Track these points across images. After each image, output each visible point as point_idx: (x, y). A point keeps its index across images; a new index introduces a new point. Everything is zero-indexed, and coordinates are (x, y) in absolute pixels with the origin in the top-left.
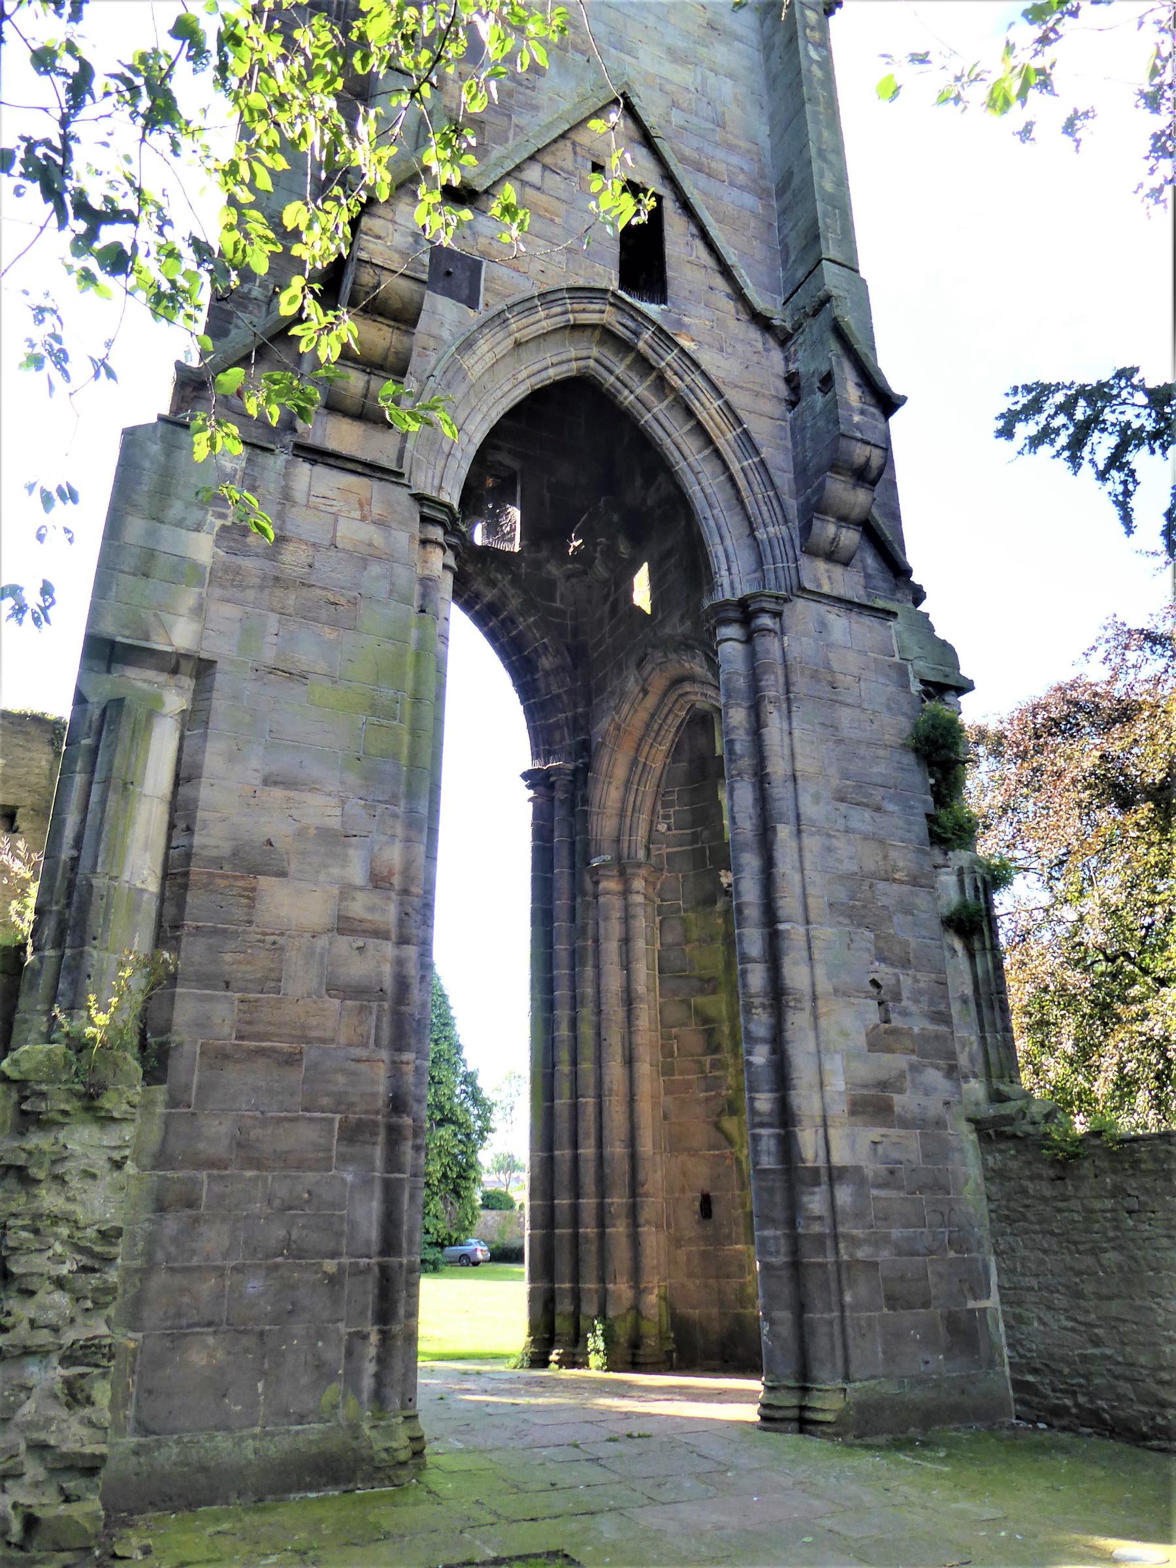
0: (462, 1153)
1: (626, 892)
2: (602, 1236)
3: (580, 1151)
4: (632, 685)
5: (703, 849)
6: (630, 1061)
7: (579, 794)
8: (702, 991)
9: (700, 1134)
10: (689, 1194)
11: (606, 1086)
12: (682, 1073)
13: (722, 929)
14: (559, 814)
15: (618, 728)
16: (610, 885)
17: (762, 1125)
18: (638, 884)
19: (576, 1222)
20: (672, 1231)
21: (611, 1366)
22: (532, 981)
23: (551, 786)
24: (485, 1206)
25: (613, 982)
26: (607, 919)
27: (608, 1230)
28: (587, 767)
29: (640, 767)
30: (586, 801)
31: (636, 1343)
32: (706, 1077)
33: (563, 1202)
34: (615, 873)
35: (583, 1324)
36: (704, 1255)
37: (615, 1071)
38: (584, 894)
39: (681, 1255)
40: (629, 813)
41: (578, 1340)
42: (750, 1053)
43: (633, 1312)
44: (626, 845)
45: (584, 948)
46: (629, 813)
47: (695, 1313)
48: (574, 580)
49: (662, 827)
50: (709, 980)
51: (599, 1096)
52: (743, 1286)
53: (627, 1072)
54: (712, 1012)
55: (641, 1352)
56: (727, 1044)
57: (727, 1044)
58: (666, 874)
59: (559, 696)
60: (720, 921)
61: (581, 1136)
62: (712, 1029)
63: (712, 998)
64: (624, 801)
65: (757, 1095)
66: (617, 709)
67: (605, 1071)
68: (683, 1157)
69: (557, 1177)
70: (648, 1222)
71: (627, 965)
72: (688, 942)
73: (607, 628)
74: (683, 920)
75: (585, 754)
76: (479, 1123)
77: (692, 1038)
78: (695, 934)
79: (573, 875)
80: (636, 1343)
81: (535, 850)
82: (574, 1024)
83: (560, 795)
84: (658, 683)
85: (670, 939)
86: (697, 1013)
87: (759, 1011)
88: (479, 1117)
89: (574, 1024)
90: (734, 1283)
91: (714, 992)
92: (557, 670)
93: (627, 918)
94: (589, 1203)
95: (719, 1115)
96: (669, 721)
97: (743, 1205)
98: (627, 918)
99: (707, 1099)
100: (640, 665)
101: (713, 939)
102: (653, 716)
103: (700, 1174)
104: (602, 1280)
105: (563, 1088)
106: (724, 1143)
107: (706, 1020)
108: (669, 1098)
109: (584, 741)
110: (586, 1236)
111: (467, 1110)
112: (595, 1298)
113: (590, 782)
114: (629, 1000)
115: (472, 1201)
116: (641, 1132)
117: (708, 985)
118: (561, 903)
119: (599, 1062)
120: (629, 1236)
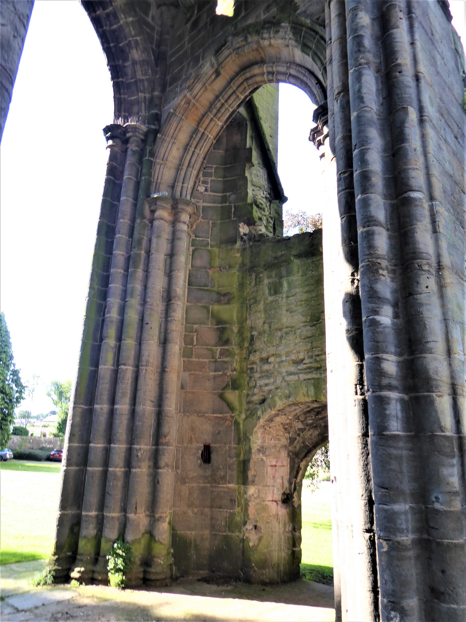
0: (6, 408)
1: (175, 222)
2: (128, 475)
3: (116, 406)
4: (207, 68)
5: (230, 207)
6: (164, 342)
7: (148, 148)
8: (219, 302)
9: (207, 401)
10: (195, 445)
11: (144, 359)
12: (198, 356)
13: (240, 260)
14: (130, 160)
15: (188, 102)
16: (163, 213)
17: (390, 387)
18: (185, 217)
19: (106, 463)
20: (179, 471)
21: (126, 585)
22: (92, 275)
23: (126, 141)
24: (14, 433)
25: (158, 283)
26: (158, 237)
27: (134, 470)
28: (156, 132)
29: (199, 135)
30: (152, 154)
31: (147, 562)
32: (216, 361)
33: (97, 445)
34: (169, 206)
35: (104, 546)
36: (203, 490)
37: (152, 349)
38: (143, 217)
39: (185, 489)
40: (185, 167)
41: (98, 558)
42: (376, 312)
43: (147, 536)
44: (179, 189)
45: (139, 255)
46: (185, 167)
47: (191, 534)
48: (164, 8)
49: (201, 189)
50: (225, 295)
51: (137, 366)
52: (232, 515)
53: (160, 350)
54: (225, 316)
55: (152, 570)
56: (235, 339)
57: (235, 339)
58: (200, 219)
59: (142, 81)
60: (238, 255)
61: (119, 394)
62: (224, 328)
63: (227, 307)
64: (182, 159)
65: (385, 356)
66: (190, 88)
67: (144, 347)
68: (194, 417)
69: (95, 425)
70: (167, 465)
71: (170, 274)
72: (211, 267)
73: (187, 39)
74: (210, 252)
75: (156, 126)
76: (18, 394)
77: (208, 333)
78: (217, 263)
79: (135, 205)
80: (147, 562)
81: (108, 182)
82: (122, 310)
83: (133, 147)
84: (230, 68)
85: (198, 263)
86: (213, 316)
87: (385, 273)
88: (17, 391)
89: (122, 310)
90: (225, 513)
91: (228, 302)
92: (143, 63)
93: (173, 240)
94: (119, 448)
95: (224, 389)
96: (230, 102)
97: (238, 455)
98: (173, 240)
99: (215, 377)
100: (218, 52)
101: (230, 267)
102: (217, 97)
103: (205, 431)
104: (124, 510)
105: (108, 358)
106: (226, 408)
107: (219, 322)
108: (187, 374)
109: (157, 114)
110: (115, 474)
111: (12, 388)
112: (117, 525)
113: (158, 141)
114: (168, 298)
115: (7, 431)
116: (168, 395)
117: (224, 297)
118: (123, 222)
119: (140, 342)
120: (150, 475)
